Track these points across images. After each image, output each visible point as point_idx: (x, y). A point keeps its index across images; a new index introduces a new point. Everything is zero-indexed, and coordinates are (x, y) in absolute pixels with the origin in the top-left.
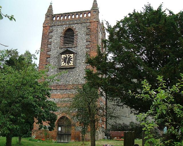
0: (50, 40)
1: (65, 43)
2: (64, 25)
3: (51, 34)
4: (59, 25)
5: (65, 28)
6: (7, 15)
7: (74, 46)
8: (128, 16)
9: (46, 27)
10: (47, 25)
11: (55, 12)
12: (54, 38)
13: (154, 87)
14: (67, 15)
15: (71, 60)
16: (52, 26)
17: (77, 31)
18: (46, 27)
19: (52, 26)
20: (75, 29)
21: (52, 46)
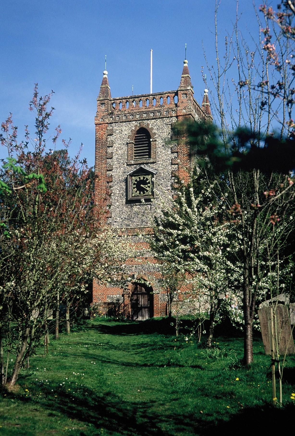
0: (110, 150)
1: (138, 154)
2: (133, 121)
3: (110, 138)
4: (123, 122)
5: (134, 126)
6: (236, 90)
7: (151, 160)
8: (58, 151)
9: (100, 124)
10: (101, 121)
11: (114, 95)
12: (116, 145)
13: (263, 363)
14: (136, 99)
15: (142, 193)
16: (111, 123)
17: (155, 134)
18: (100, 124)
19: (111, 123)
20: (152, 129)
21: (114, 162)
